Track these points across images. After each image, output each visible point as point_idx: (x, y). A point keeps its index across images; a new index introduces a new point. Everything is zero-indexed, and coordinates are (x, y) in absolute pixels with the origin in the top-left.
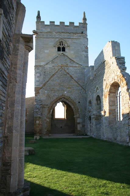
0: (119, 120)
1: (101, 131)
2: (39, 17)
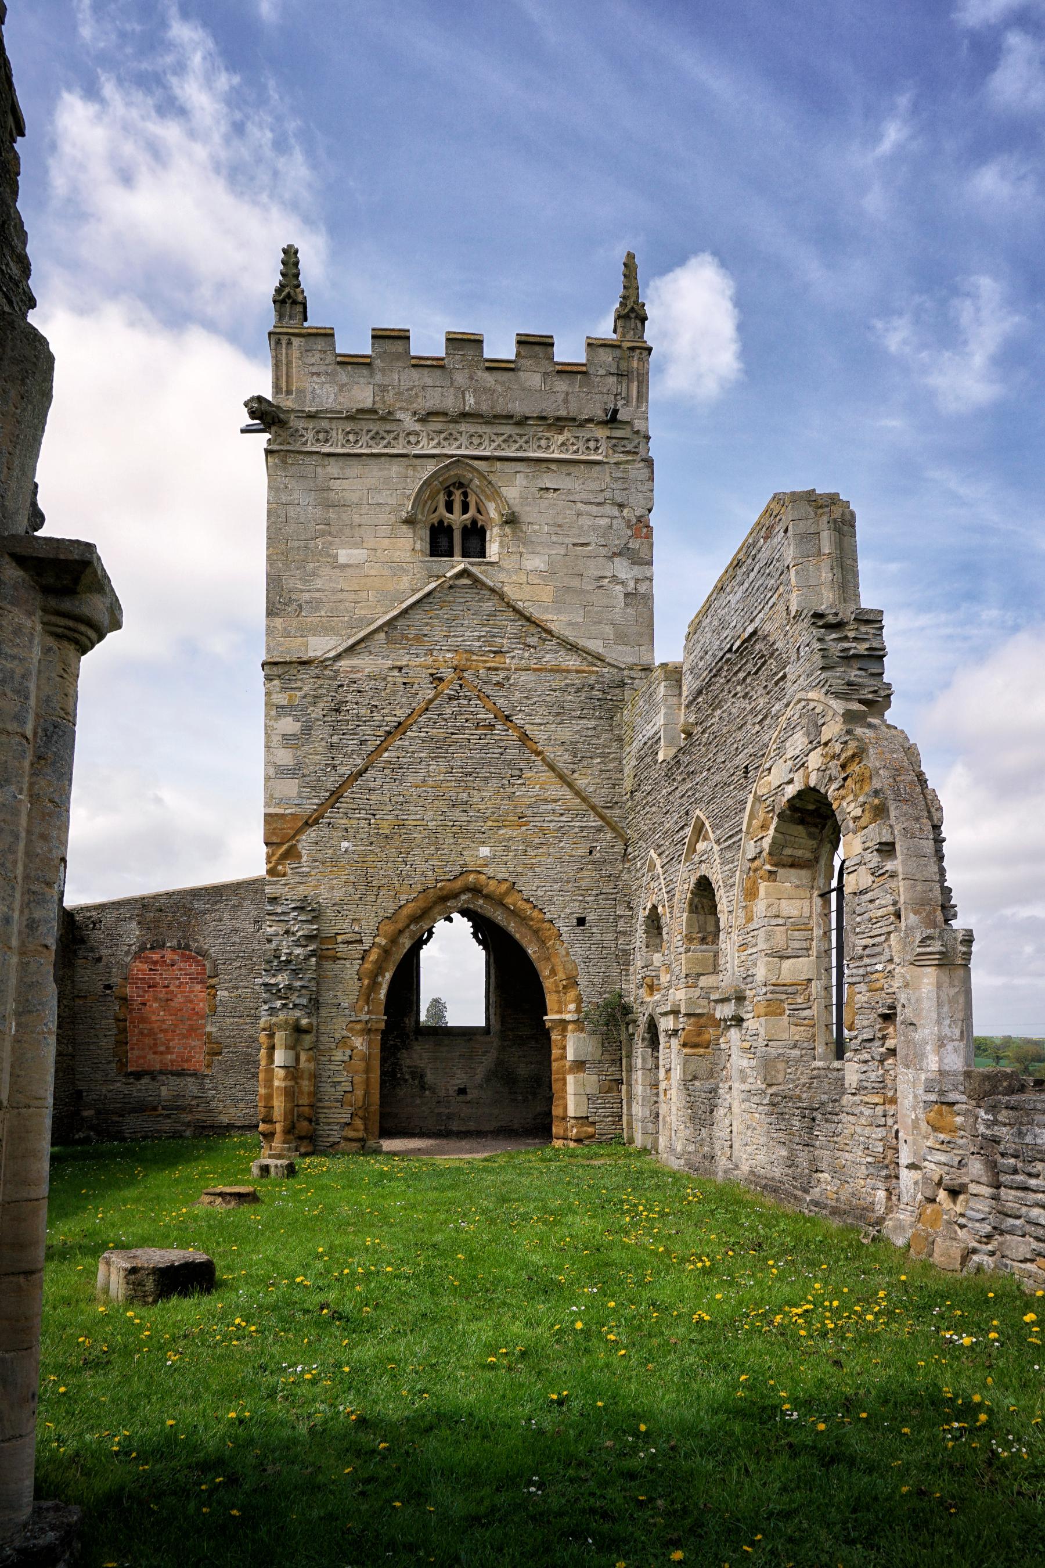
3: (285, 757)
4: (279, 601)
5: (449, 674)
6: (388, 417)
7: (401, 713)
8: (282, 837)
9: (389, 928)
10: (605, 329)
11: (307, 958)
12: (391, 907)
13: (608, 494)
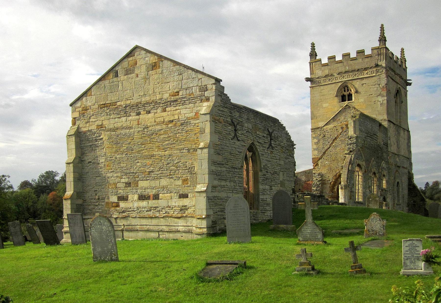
0: (357, 200)
1: (226, 221)
2: (313, 54)
3: (315, 147)
4: (313, 117)
5: (344, 126)
6: (332, 75)
7: (336, 136)
8: (316, 162)
9: (335, 178)
10: (377, 44)
11: (319, 184)
12: (335, 174)
13: (376, 82)
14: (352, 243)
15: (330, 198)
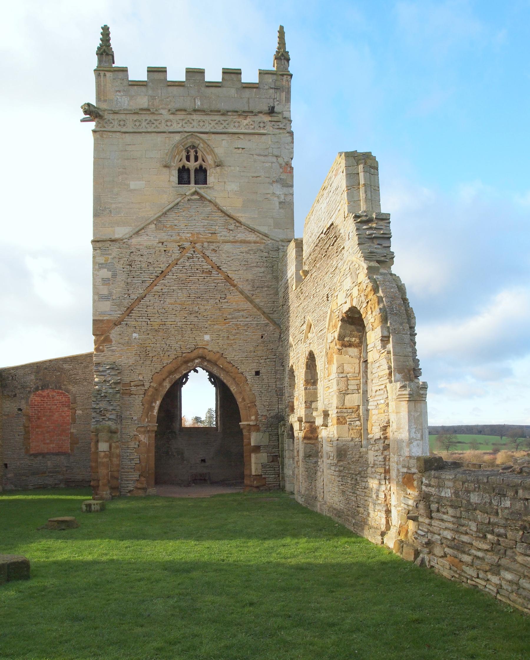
2: (105, 52)
7: (163, 267)
8: (102, 329)
12: (159, 367)
14: (498, 540)
15: (144, 433)
